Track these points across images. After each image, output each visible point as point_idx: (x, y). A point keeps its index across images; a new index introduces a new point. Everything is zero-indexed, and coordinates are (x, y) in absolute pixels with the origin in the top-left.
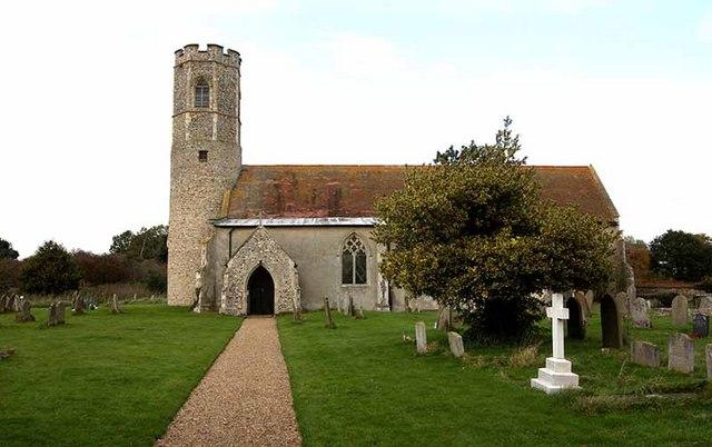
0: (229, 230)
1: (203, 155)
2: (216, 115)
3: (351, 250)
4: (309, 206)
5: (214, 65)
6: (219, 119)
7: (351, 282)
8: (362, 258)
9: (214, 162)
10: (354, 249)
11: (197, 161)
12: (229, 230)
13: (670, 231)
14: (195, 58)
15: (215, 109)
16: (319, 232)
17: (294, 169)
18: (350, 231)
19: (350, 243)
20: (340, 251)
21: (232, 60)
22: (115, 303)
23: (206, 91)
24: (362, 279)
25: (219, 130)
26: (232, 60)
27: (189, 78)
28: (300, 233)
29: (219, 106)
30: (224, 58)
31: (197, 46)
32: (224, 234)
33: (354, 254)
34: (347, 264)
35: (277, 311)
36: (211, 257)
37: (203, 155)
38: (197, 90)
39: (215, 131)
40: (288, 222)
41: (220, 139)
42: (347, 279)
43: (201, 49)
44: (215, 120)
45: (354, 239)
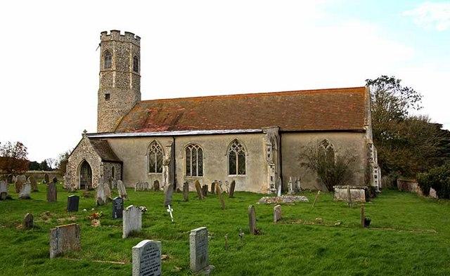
3: (235, 151)
4: (160, 124)
5: (114, 43)
15: (114, 69)
16: (137, 141)
17: (171, 103)
18: (152, 140)
19: (234, 146)
21: (132, 41)
25: (117, 81)
26: (132, 41)
28: (126, 141)
29: (117, 67)
34: (232, 157)
39: (114, 81)
40: (146, 134)
41: (118, 86)
42: (152, 170)
44: (114, 75)
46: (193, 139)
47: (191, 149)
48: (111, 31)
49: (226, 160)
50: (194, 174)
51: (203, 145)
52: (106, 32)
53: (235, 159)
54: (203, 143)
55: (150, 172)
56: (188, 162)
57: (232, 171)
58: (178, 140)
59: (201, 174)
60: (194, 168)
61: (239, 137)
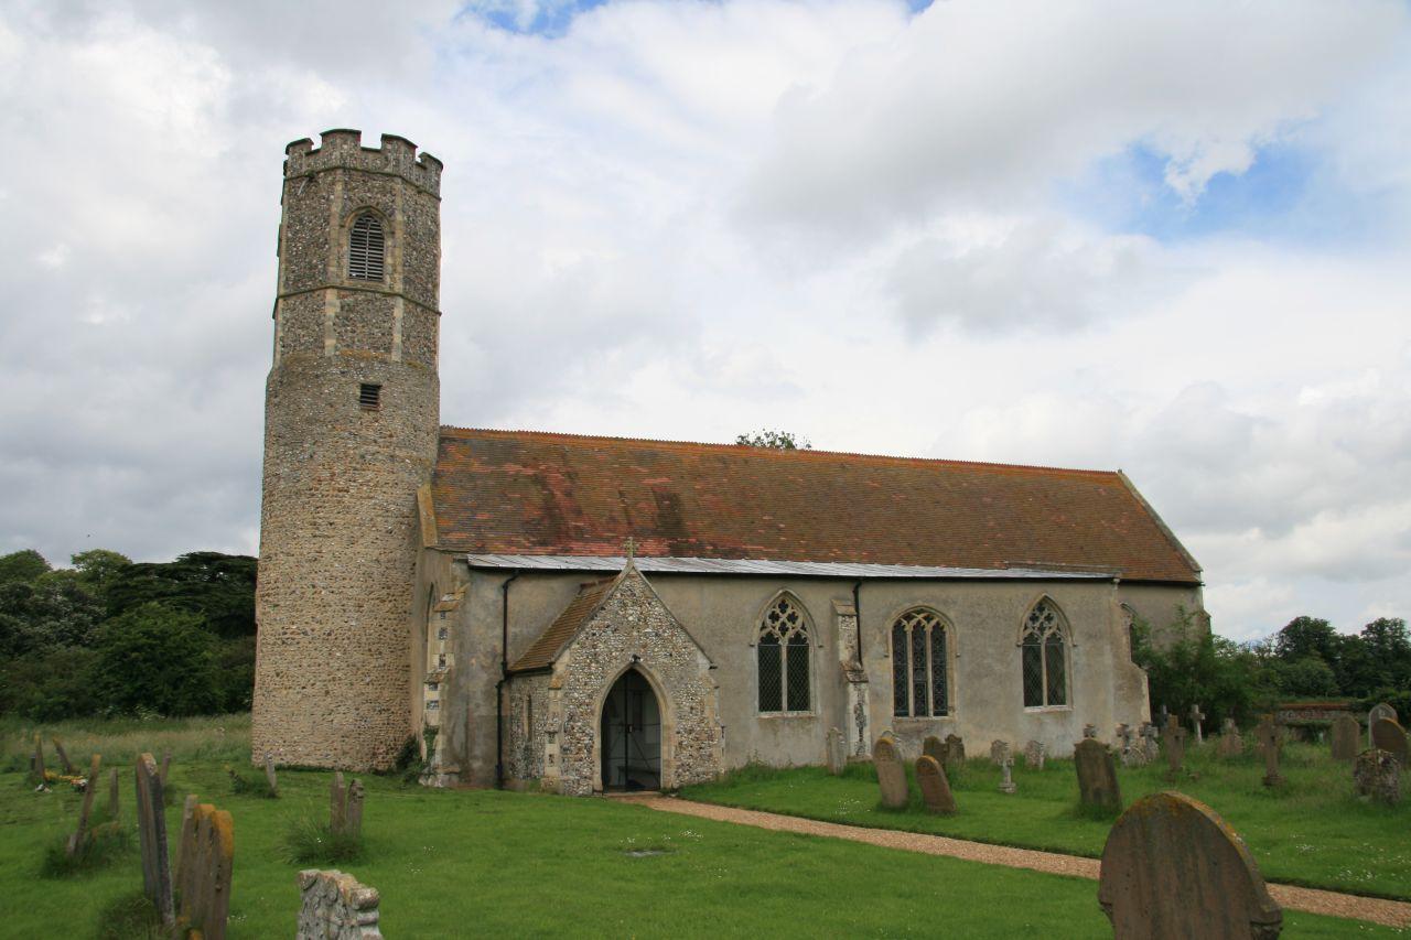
0: (855, 585)
1: (370, 394)
2: (400, 301)
3: (777, 632)
6: (407, 312)
7: (779, 708)
8: (799, 649)
9: (393, 417)
10: (784, 629)
11: (355, 408)
12: (501, 580)
13: (1325, 623)
14: (350, 163)
15: (399, 287)
16: (711, 592)
18: (777, 590)
20: (756, 636)
22: (885, 842)
23: (378, 242)
24: (800, 701)
25: (407, 338)
27: (336, 208)
29: (407, 281)
30: (416, 171)
31: (357, 134)
32: (490, 591)
33: (784, 643)
35: (669, 778)
36: (461, 646)
37: (370, 394)
38: (357, 240)
39: (397, 338)
42: (769, 701)
43: (365, 142)
44: (399, 312)
45: (783, 607)
46: (921, 596)
47: (909, 627)
48: (324, 135)
49: (1017, 660)
50: (921, 711)
51: (951, 614)
52: (306, 142)
53: (1038, 658)
54: (954, 606)
55: (763, 708)
56: (899, 671)
57: (1032, 698)
58: (868, 595)
59: (942, 707)
60: (920, 689)
61: (1054, 592)
